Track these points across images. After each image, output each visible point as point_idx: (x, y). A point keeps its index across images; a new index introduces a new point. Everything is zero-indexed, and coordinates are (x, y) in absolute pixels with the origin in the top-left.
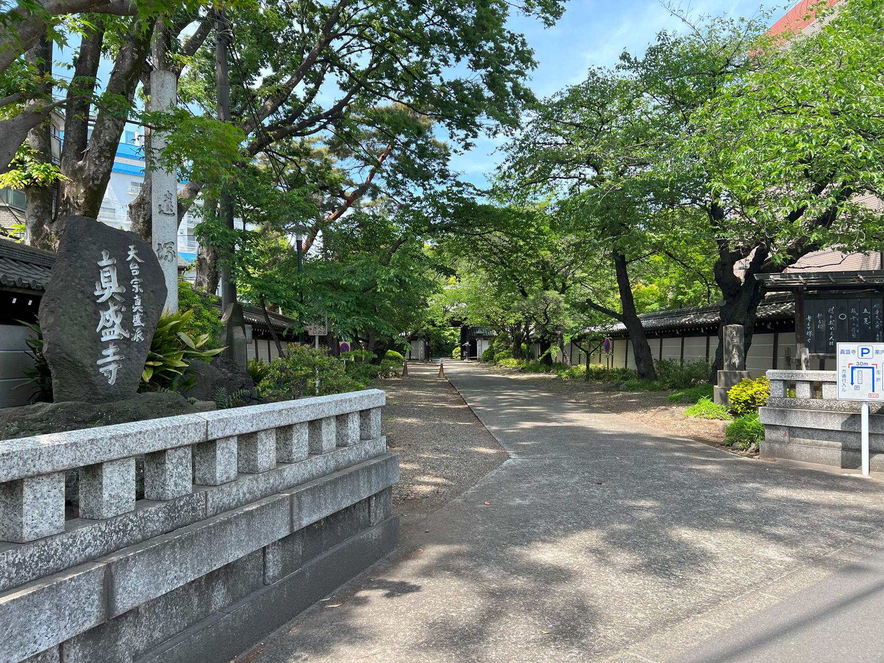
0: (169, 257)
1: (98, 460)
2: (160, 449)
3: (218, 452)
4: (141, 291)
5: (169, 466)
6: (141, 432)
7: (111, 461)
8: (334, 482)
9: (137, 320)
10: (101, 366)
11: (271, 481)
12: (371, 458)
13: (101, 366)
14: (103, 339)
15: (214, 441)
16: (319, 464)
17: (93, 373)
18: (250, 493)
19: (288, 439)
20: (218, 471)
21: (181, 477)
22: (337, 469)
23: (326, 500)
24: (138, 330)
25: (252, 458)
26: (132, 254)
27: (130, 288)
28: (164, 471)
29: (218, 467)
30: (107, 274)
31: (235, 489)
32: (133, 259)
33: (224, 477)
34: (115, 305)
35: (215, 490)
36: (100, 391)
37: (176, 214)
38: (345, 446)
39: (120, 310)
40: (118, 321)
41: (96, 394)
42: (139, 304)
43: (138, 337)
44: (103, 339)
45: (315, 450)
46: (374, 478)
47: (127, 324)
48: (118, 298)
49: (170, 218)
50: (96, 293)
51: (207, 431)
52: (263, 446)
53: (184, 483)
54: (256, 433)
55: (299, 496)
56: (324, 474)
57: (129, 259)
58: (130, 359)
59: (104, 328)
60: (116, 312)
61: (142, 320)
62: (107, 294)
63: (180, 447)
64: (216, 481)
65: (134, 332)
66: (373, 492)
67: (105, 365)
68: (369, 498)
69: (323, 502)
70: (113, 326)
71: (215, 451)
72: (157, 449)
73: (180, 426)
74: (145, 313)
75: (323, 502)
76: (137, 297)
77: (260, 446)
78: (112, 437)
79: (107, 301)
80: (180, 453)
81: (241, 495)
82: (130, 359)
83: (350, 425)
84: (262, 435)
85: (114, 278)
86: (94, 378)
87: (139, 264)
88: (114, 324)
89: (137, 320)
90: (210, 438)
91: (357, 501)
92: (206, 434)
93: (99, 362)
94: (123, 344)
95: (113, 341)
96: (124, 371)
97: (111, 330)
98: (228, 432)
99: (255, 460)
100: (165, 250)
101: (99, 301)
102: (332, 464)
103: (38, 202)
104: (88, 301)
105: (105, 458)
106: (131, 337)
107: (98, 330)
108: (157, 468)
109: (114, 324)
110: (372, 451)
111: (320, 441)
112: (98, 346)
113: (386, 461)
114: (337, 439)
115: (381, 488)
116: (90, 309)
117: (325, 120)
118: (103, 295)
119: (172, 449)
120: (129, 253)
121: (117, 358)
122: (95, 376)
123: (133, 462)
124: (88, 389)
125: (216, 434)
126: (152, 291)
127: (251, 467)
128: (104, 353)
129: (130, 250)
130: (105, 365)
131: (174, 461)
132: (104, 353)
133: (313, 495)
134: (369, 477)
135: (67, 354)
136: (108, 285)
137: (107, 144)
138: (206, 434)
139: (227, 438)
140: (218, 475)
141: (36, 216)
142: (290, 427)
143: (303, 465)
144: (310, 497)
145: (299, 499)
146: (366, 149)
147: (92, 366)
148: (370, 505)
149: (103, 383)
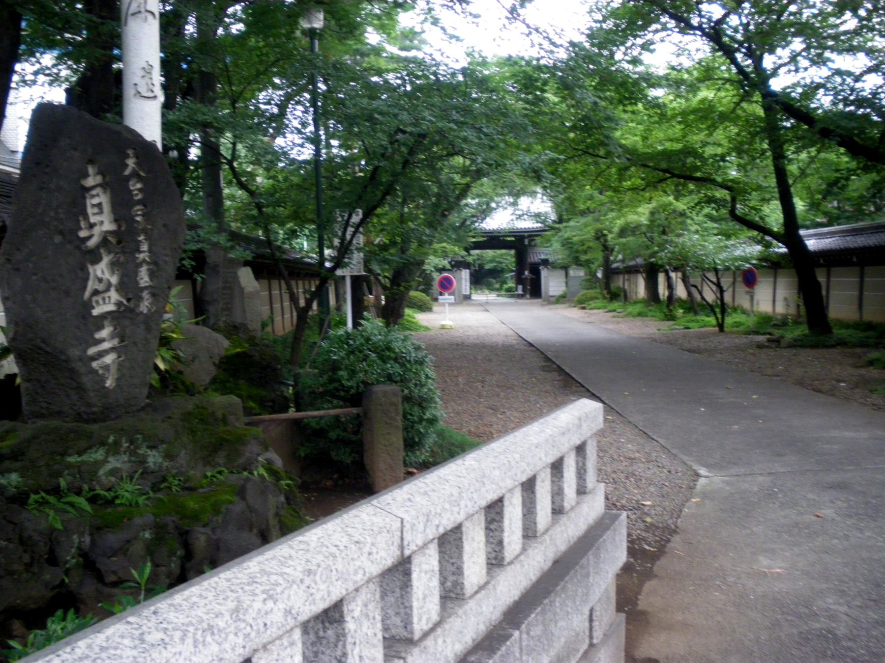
40: (114, 280)
44: (95, 312)
57: (127, 172)
70: (108, 290)
79: (98, 247)
89: (144, 278)
92: (402, 547)
93: (92, 351)
128: (98, 336)
132: (98, 336)
147: (80, 360)
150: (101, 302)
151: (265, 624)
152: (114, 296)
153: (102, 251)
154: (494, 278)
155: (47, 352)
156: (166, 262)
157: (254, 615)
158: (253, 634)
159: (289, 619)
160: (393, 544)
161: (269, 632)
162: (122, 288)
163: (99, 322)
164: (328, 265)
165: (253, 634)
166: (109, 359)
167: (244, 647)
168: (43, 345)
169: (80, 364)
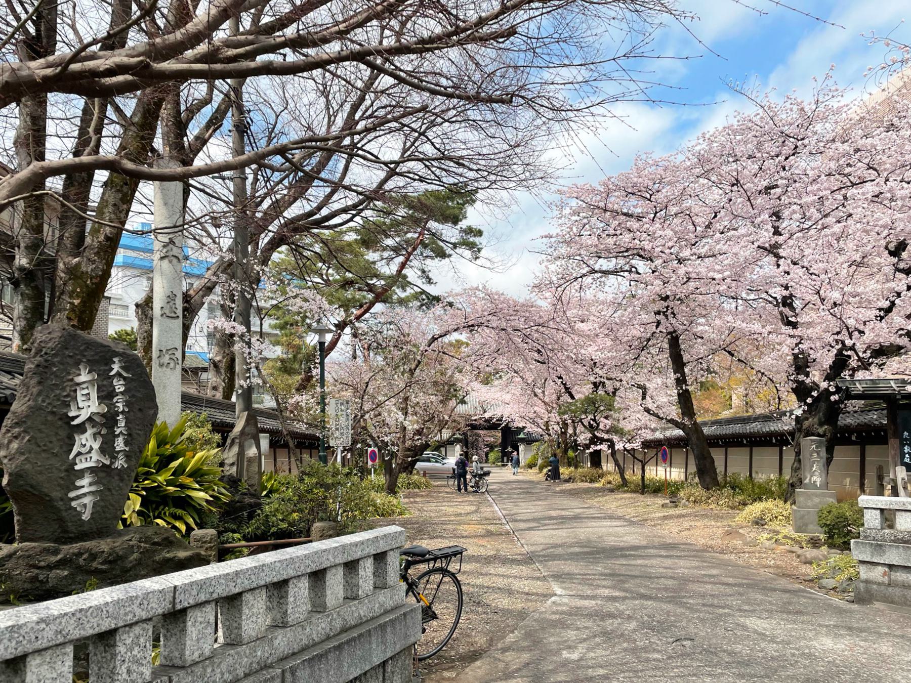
0: (172, 365)
1: (20, 651)
2: (109, 628)
3: (189, 624)
4: (127, 410)
5: (121, 649)
6: (81, 610)
7: (39, 651)
8: (339, 647)
9: (120, 444)
10: (73, 499)
11: (259, 654)
12: (386, 612)
13: (73, 499)
14: (76, 468)
15: (184, 611)
16: (321, 627)
17: (62, 508)
18: (230, 672)
19: (282, 597)
20: (188, 647)
21: (138, 662)
22: (344, 630)
23: (328, 672)
24: (121, 456)
25: (235, 625)
26: (116, 368)
27: (111, 406)
28: (114, 656)
29: (188, 643)
30: (85, 392)
31: (209, 670)
32: (119, 374)
33: (196, 654)
34: (93, 427)
35: (182, 673)
36: (73, 529)
37: (181, 316)
38: (354, 599)
39: (99, 433)
40: (96, 446)
41: (66, 532)
42: (123, 425)
43: (120, 463)
44: (76, 468)
45: (318, 607)
46: (389, 637)
47: (107, 448)
48: (97, 419)
49: (173, 321)
50: (71, 414)
51: (174, 598)
52: (250, 609)
53: (141, 669)
54: (240, 594)
55: (293, 671)
56: (328, 638)
57: (112, 373)
58: (110, 490)
59: (79, 454)
60: (95, 435)
61: (126, 444)
62: (84, 415)
63: (136, 623)
64: (184, 661)
65: (116, 458)
66: (389, 655)
67: (78, 497)
68: (384, 664)
69: (324, 675)
70: (90, 452)
71: (184, 622)
72: (104, 629)
73: (136, 597)
74: (129, 435)
75: (324, 675)
76: (121, 417)
77: (246, 611)
78: (41, 621)
79: (83, 423)
80: (137, 630)
81: (219, 676)
82: (110, 490)
83: (361, 572)
84: (248, 597)
85: (94, 395)
86: (64, 514)
87: (125, 378)
88: (91, 449)
89: (120, 444)
90: (178, 607)
91: (367, 668)
92: (173, 603)
93: (72, 495)
94: (101, 472)
95: (91, 470)
96: (102, 504)
97: (88, 456)
98: (203, 598)
99: (239, 627)
100: (167, 357)
101: (75, 423)
102: (338, 624)
103: (28, 303)
104: (60, 423)
105: (29, 648)
106: (112, 463)
107: (71, 457)
108: (106, 652)
109: (91, 449)
110: (390, 604)
111: (324, 595)
112: (72, 475)
113: (405, 614)
114: (346, 590)
115: (398, 648)
116: (63, 433)
117: (354, 212)
118: (77, 417)
119: (125, 626)
120: (113, 366)
121: (93, 488)
122: (66, 511)
123: (70, 649)
124: (57, 527)
125: (184, 601)
126: (140, 410)
127: (233, 636)
128: (79, 483)
129: (114, 362)
130: (78, 497)
131: (129, 641)
132: (79, 483)
133: (311, 667)
134: (383, 636)
135: (32, 486)
136: (87, 404)
137: (107, 238)
138: (173, 603)
139: (200, 605)
140: (187, 653)
141: (26, 319)
142: (285, 582)
143: (300, 629)
144: (308, 671)
145: (293, 674)
146: (571, 123)
147: (62, 500)
148: (384, 671)
149: (73, 519)
150: (83, 461)
151: (37, 637)
152: (95, 456)
153: (87, 425)
154: (591, 464)
155: (34, 495)
156: (138, 434)
157: (28, 630)
158: (25, 642)
159: (59, 636)
160: (164, 600)
161: (39, 642)
162: (103, 450)
163: (81, 474)
164: (510, 449)
165: (25, 642)
166: (87, 500)
167: (16, 649)
168: (30, 489)
169: (61, 503)
